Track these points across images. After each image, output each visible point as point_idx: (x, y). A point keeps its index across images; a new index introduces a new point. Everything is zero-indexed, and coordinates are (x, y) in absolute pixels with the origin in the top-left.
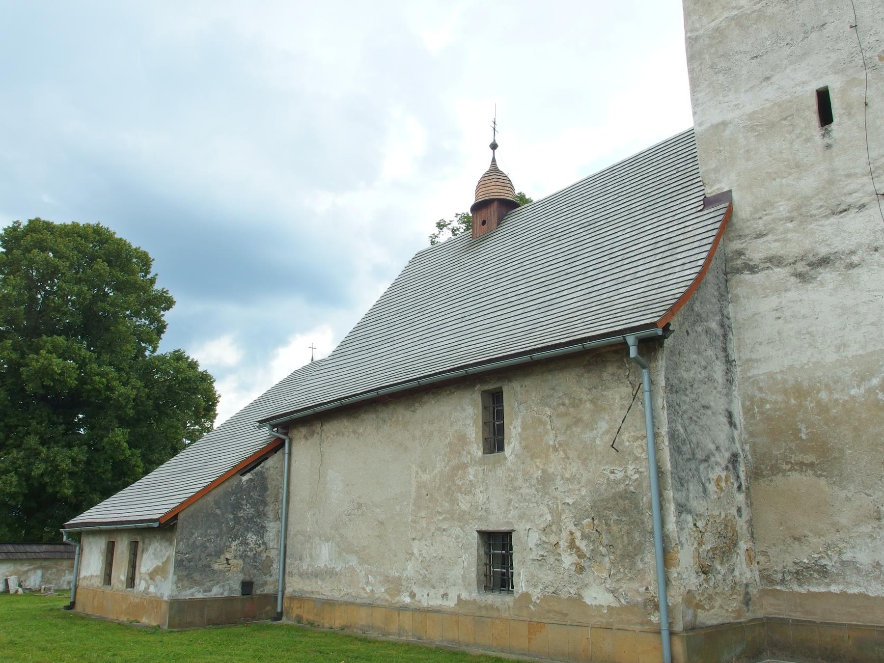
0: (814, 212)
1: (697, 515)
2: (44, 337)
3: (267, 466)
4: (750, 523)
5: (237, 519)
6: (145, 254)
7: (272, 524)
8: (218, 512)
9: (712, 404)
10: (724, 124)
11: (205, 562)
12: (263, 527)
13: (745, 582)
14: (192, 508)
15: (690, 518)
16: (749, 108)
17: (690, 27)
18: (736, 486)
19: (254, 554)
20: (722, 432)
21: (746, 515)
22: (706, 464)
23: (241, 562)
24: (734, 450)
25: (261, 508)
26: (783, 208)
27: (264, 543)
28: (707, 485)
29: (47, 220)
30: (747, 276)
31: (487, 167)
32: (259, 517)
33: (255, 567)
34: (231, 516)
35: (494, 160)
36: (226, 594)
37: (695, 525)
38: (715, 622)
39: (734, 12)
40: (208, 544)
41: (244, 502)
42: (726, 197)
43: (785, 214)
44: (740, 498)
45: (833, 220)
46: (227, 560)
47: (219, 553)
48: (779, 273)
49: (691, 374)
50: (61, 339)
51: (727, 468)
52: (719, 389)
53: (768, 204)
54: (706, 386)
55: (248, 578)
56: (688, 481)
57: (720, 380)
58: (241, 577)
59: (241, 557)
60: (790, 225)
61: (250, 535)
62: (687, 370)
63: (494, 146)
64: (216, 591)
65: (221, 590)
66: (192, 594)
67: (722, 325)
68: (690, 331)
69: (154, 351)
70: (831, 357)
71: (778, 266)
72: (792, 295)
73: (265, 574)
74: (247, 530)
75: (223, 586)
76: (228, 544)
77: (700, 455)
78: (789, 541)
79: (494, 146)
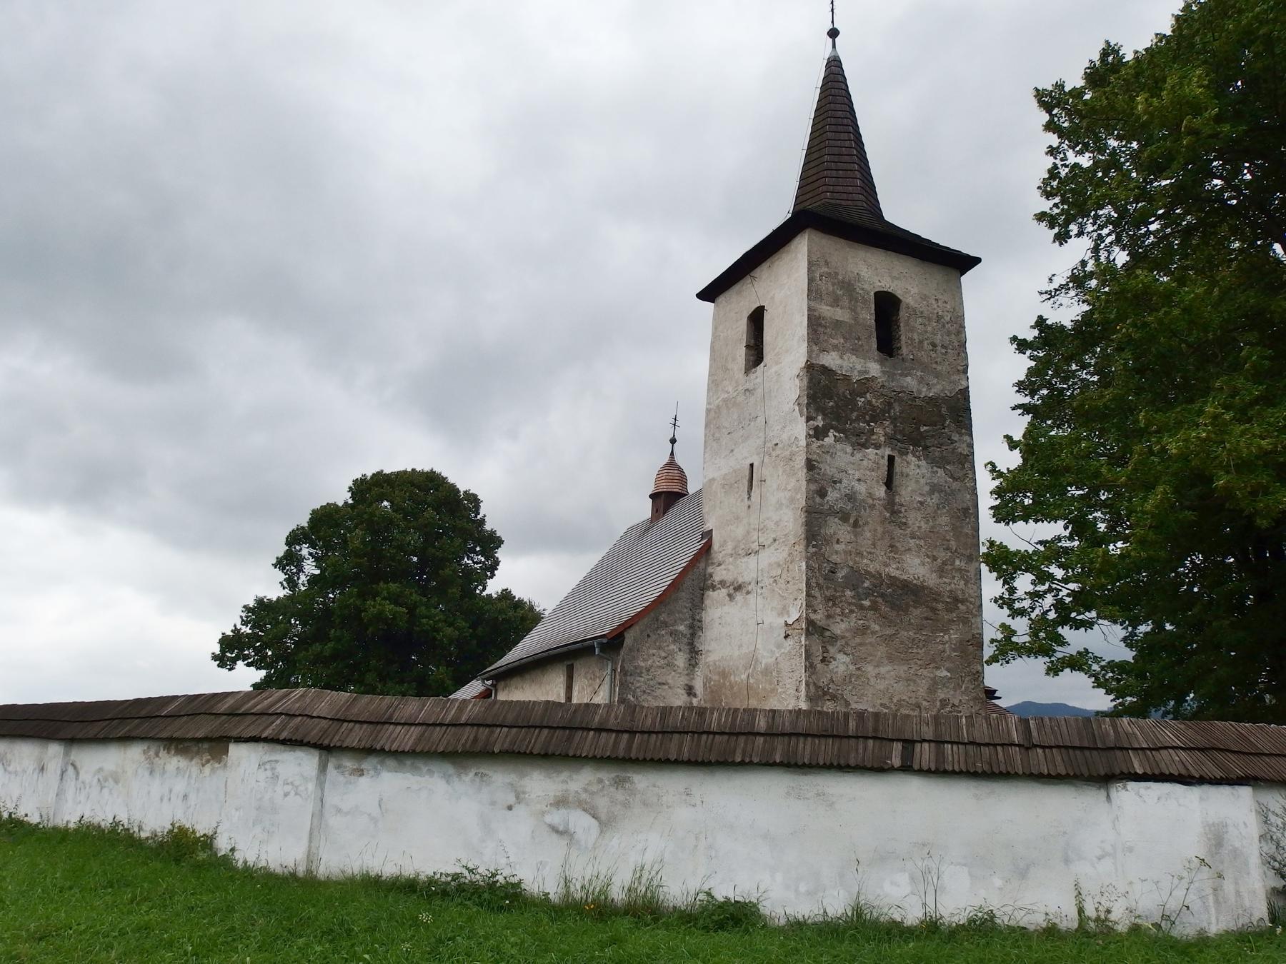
2: (381, 584)
6: (475, 496)
10: (713, 479)
16: (724, 471)
17: (709, 403)
26: (730, 546)
30: (711, 593)
31: (666, 459)
35: (672, 453)
42: (709, 533)
45: (746, 559)
48: (724, 592)
50: (393, 587)
57: (682, 665)
62: (645, 660)
63: (673, 441)
67: (691, 627)
69: (484, 589)
70: (737, 653)
72: (726, 609)
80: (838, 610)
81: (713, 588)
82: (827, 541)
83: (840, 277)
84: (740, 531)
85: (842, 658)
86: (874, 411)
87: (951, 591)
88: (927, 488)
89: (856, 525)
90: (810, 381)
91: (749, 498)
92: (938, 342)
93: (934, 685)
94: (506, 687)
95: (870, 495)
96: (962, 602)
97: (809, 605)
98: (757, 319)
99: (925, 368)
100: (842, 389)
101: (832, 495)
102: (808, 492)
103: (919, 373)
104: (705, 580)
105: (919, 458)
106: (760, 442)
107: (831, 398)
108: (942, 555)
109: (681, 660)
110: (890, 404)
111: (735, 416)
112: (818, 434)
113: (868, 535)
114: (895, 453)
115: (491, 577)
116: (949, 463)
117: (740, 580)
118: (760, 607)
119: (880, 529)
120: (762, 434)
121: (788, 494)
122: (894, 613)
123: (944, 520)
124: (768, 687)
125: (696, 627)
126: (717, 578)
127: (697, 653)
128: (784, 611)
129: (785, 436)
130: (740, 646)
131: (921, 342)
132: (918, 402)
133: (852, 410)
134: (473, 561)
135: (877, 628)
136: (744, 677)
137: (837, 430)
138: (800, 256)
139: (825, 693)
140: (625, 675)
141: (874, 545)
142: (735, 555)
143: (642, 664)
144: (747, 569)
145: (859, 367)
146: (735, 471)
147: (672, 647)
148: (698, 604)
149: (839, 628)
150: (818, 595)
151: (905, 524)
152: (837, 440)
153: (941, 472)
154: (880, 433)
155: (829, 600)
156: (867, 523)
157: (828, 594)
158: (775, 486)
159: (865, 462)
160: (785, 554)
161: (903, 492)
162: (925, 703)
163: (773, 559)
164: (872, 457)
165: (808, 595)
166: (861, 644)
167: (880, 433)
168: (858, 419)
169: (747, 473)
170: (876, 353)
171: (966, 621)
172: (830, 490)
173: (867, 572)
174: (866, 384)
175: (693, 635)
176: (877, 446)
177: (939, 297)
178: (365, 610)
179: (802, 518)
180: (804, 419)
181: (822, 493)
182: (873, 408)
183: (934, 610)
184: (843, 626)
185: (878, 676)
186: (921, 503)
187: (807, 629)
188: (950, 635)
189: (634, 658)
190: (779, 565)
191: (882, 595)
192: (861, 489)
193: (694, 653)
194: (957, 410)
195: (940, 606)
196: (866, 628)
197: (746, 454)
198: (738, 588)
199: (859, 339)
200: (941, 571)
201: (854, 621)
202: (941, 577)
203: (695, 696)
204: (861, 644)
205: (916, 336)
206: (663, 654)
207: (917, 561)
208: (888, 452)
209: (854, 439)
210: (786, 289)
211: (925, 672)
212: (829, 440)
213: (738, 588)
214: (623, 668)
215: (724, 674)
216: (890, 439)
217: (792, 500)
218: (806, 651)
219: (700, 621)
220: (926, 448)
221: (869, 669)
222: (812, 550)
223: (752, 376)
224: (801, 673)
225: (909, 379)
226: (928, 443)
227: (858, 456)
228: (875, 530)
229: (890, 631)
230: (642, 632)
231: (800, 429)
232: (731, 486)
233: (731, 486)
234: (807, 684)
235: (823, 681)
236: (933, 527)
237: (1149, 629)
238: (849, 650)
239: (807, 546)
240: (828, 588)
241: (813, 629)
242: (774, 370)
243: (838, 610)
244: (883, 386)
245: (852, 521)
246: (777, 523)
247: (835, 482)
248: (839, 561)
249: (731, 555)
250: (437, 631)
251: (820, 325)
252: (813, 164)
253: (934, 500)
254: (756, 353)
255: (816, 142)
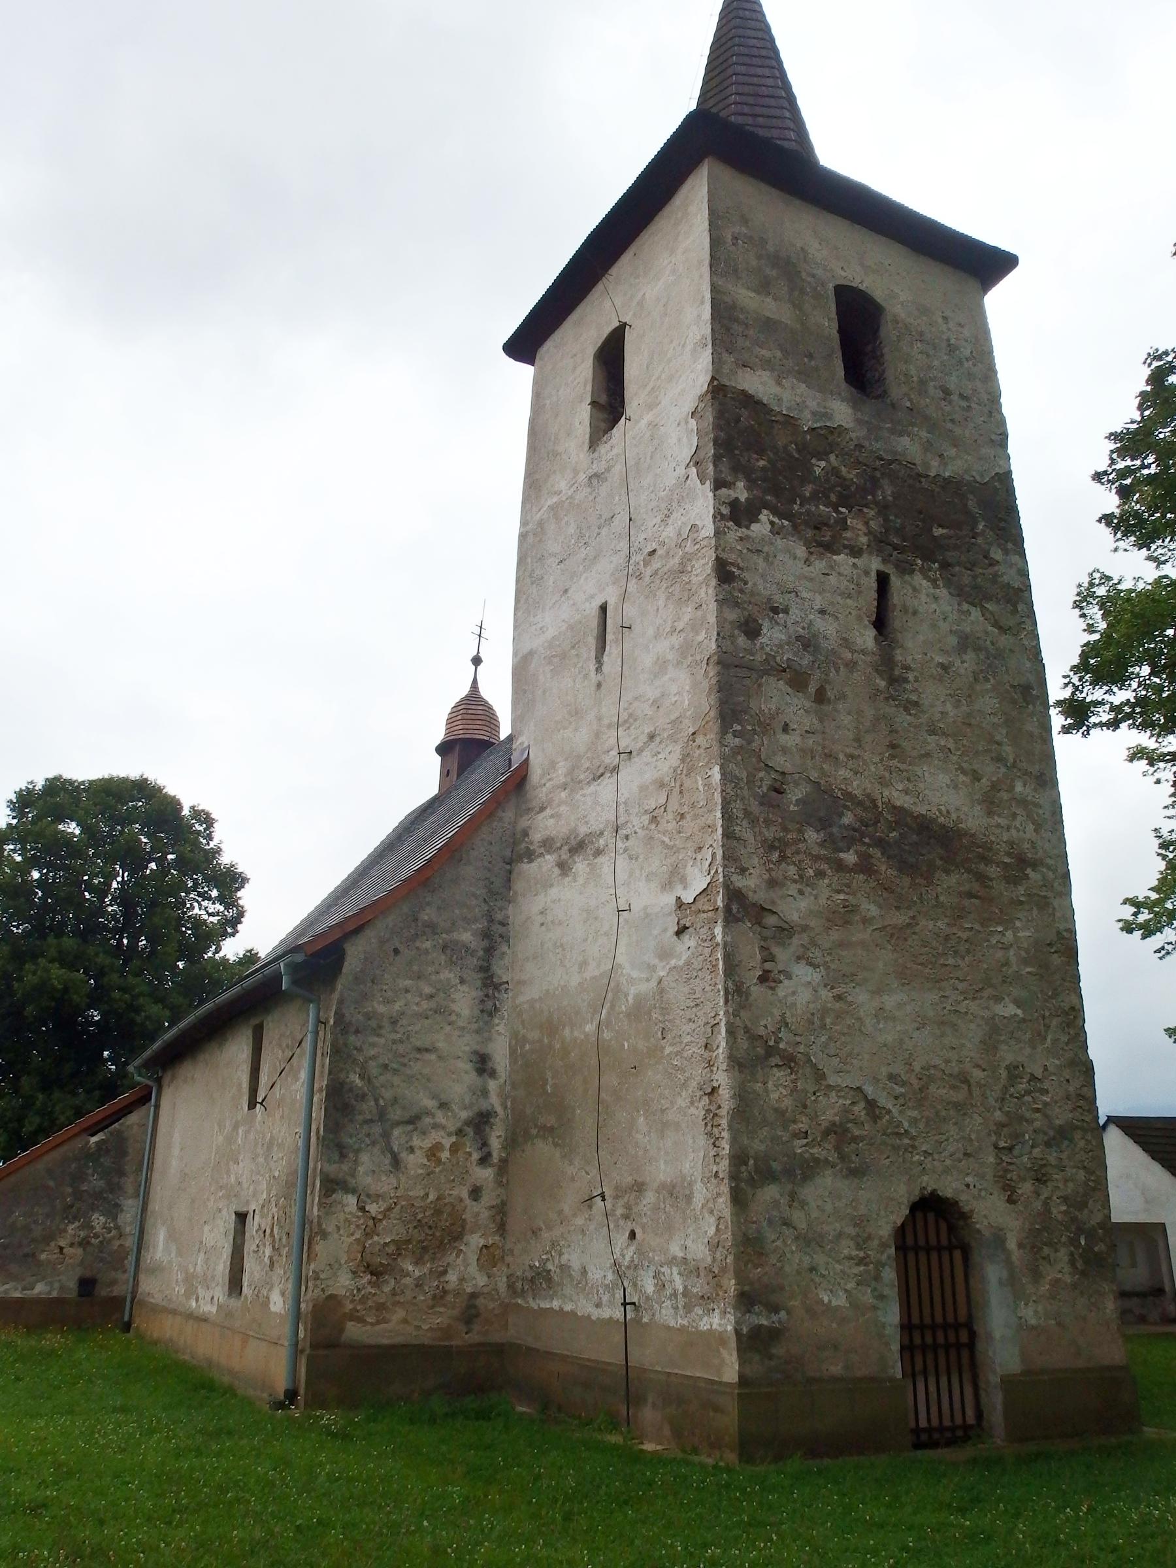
0: (582, 777)
1: (368, 1196)
3: (128, 1123)
4: (501, 1212)
5: (78, 1195)
6: (208, 814)
7: (130, 1202)
8: (51, 1183)
9: (440, 1045)
11: (26, 1250)
12: (117, 1205)
13: (469, 1290)
14: (12, 1179)
15: (351, 1200)
16: (551, 633)
18: (476, 1156)
19: (101, 1242)
20: (459, 1084)
21: (489, 1198)
22: (411, 1127)
23: (80, 1251)
24: (484, 1105)
25: (116, 1180)
26: (562, 768)
27: (117, 1227)
28: (404, 1155)
29: (94, 776)
30: (525, 866)
31: (464, 691)
32: (112, 1191)
33: (102, 1260)
34: (70, 1190)
35: (475, 681)
36: (55, 1294)
37: (363, 1209)
38: (385, 1341)
39: (555, 499)
40: (33, 1226)
41: (90, 1171)
43: (562, 780)
44: (485, 1175)
45: (592, 788)
46: (61, 1249)
47: (48, 1238)
49: (397, 1006)
51: (459, 1132)
52: (460, 1023)
53: (553, 765)
54: (427, 1022)
55: (88, 1274)
56: (357, 1152)
58: (79, 1272)
59: (80, 1244)
60: (563, 795)
61: (96, 1216)
62: (387, 1001)
63: (477, 661)
64: (40, 1289)
65: (48, 1288)
66: (6, 1292)
67: (486, 935)
68: (401, 948)
69: (218, 951)
70: (575, 981)
71: (549, 852)
73: (116, 1270)
74: (93, 1208)
75: (51, 1283)
76: (62, 1226)
77: (395, 1114)
78: (529, 1234)
79: (477, 661)
80: (792, 870)
81: (530, 856)
82: (765, 726)
83: (770, 248)
84: (580, 737)
85: (803, 973)
86: (847, 488)
87: (1011, 844)
88: (953, 641)
89: (820, 697)
90: (720, 415)
91: (599, 670)
92: (952, 387)
93: (994, 1035)
94: (174, 1077)
95: (846, 642)
96: (1034, 865)
97: (729, 857)
98: (611, 357)
99: (933, 427)
100: (782, 439)
101: (772, 635)
102: (721, 622)
103: (924, 434)
104: (515, 843)
105: (934, 582)
106: (619, 559)
107: (761, 452)
108: (990, 771)
109: (464, 1001)
110: (875, 482)
111: (572, 530)
112: (736, 514)
113: (846, 720)
114: (889, 569)
115: (233, 935)
116: (989, 598)
117: (583, 830)
118: (622, 877)
119: (869, 712)
120: (623, 545)
121: (676, 640)
122: (907, 881)
123: (988, 703)
124: (641, 1045)
125: (495, 937)
126: (537, 836)
127: (497, 987)
128: (675, 876)
129: (669, 533)
130: (583, 964)
131: (922, 382)
132: (925, 483)
133: (804, 481)
134: (206, 910)
135: (873, 910)
136: (590, 1028)
137: (775, 511)
138: (692, 209)
139: (770, 1051)
140: (345, 1032)
141: (858, 740)
142: (572, 784)
143: (382, 1009)
144: (594, 808)
145: (812, 404)
146: (571, 627)
147: (447, 975)
148: (501, 888)
149: (795, 907)
150: (748, 835)
151: (916, 704)
152: (776, 531)
153: (976, 613)
154: (858, 529)
155: (772, 847)
156: (842, 697)
157: (769, 834)
158: (651, 632)
159: (833, 579)
160: (674, 760)
161: (910, 644)
162: (977, 1074)
163: (649, 776)
164: (847, 570)
165: (728, 835)
166: (842, 945)
167: (858, 529)
168: (815, 497)
169: (594, 623)
170: (844, 385)
171: (1043, 904)
172: (766, 625)
173: (849, 796)
174: (826, 439)
175: (490, 951)
176: (855, 552)
177: (948, 313)
178: (20, 979)
179: (707, 678)
180: (708, 485)
181: (751, 630)
182: (843, 482)
183: (982, 878)
184: (804, 904)
185: (880, 1013)
186: (945, 668)
187: (728, 909)
188: (1016, 930)
189: (365, 996)
190: (662, 785)
191: (880, 843)
192: (828, 628)
193: (491, 987)
194: (990, 512)
195: (993, 871)
196: (850, 910)
197: (594, 587)
198: (579, 846)
199: (811, 356)
200: (990, 803)
201: (824, 894)
202: (990, 813)
203: (493, 1074)
204: (842, 945)
205: (913, 372)
206: (428, 990)
207: (943, 779)
208: (876, 564)
209: (809, 533)
210: (670, 300)
211: (973, 1006)
212: (761, 528)
213: (579, 846)
214: (339, 1016)
215: (551, 1028)
216: (880, 543)
217: (685, 650)
218: (727, 957)
219: (503, 924)
220: (945, 565)
221: (861, 997)
222: (733, 741)
223: (603, 449)
224: (717, 1006)
225: (905, 441)
226: (951, 555)
227: (819, 565)
228: (860, 712)
229: (900, 918)
230: (382, 942)
231: (701, 508)
232: (563, 656)
233: (563, 656)
234: (731, 1032)
235: (766, 1024)
236: (969, 715)
237: (273, 1308)
238: (816, 954)
239: (723, 732)
240: (768, 823)
241: (739, 908)
242: (644, 423)
243: (792, 870)
244: (859, 447)
245: (812, 689)
246: (657, 704)
247: (775, 610)
248: (788, 767)
249: (564, 787)
250: (137, 1010)
251: (736, 320)
252: (709, 95)
253: (967, 664)
254: (610, 403)
255: (714, 83)
